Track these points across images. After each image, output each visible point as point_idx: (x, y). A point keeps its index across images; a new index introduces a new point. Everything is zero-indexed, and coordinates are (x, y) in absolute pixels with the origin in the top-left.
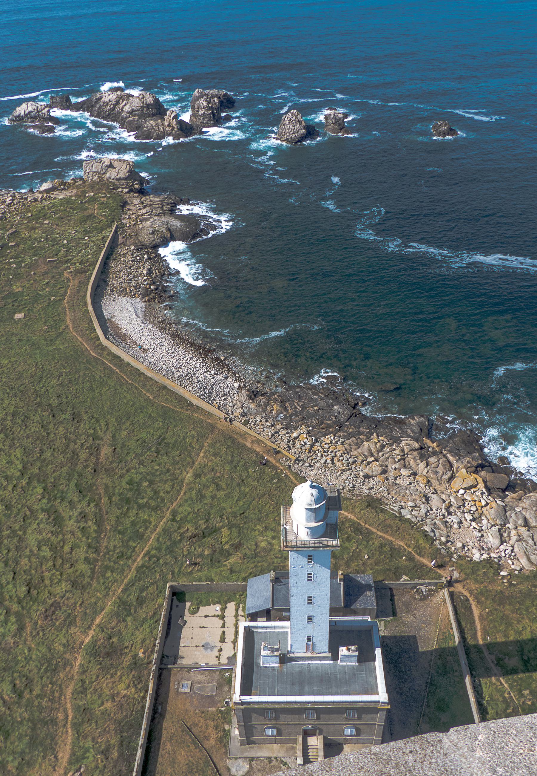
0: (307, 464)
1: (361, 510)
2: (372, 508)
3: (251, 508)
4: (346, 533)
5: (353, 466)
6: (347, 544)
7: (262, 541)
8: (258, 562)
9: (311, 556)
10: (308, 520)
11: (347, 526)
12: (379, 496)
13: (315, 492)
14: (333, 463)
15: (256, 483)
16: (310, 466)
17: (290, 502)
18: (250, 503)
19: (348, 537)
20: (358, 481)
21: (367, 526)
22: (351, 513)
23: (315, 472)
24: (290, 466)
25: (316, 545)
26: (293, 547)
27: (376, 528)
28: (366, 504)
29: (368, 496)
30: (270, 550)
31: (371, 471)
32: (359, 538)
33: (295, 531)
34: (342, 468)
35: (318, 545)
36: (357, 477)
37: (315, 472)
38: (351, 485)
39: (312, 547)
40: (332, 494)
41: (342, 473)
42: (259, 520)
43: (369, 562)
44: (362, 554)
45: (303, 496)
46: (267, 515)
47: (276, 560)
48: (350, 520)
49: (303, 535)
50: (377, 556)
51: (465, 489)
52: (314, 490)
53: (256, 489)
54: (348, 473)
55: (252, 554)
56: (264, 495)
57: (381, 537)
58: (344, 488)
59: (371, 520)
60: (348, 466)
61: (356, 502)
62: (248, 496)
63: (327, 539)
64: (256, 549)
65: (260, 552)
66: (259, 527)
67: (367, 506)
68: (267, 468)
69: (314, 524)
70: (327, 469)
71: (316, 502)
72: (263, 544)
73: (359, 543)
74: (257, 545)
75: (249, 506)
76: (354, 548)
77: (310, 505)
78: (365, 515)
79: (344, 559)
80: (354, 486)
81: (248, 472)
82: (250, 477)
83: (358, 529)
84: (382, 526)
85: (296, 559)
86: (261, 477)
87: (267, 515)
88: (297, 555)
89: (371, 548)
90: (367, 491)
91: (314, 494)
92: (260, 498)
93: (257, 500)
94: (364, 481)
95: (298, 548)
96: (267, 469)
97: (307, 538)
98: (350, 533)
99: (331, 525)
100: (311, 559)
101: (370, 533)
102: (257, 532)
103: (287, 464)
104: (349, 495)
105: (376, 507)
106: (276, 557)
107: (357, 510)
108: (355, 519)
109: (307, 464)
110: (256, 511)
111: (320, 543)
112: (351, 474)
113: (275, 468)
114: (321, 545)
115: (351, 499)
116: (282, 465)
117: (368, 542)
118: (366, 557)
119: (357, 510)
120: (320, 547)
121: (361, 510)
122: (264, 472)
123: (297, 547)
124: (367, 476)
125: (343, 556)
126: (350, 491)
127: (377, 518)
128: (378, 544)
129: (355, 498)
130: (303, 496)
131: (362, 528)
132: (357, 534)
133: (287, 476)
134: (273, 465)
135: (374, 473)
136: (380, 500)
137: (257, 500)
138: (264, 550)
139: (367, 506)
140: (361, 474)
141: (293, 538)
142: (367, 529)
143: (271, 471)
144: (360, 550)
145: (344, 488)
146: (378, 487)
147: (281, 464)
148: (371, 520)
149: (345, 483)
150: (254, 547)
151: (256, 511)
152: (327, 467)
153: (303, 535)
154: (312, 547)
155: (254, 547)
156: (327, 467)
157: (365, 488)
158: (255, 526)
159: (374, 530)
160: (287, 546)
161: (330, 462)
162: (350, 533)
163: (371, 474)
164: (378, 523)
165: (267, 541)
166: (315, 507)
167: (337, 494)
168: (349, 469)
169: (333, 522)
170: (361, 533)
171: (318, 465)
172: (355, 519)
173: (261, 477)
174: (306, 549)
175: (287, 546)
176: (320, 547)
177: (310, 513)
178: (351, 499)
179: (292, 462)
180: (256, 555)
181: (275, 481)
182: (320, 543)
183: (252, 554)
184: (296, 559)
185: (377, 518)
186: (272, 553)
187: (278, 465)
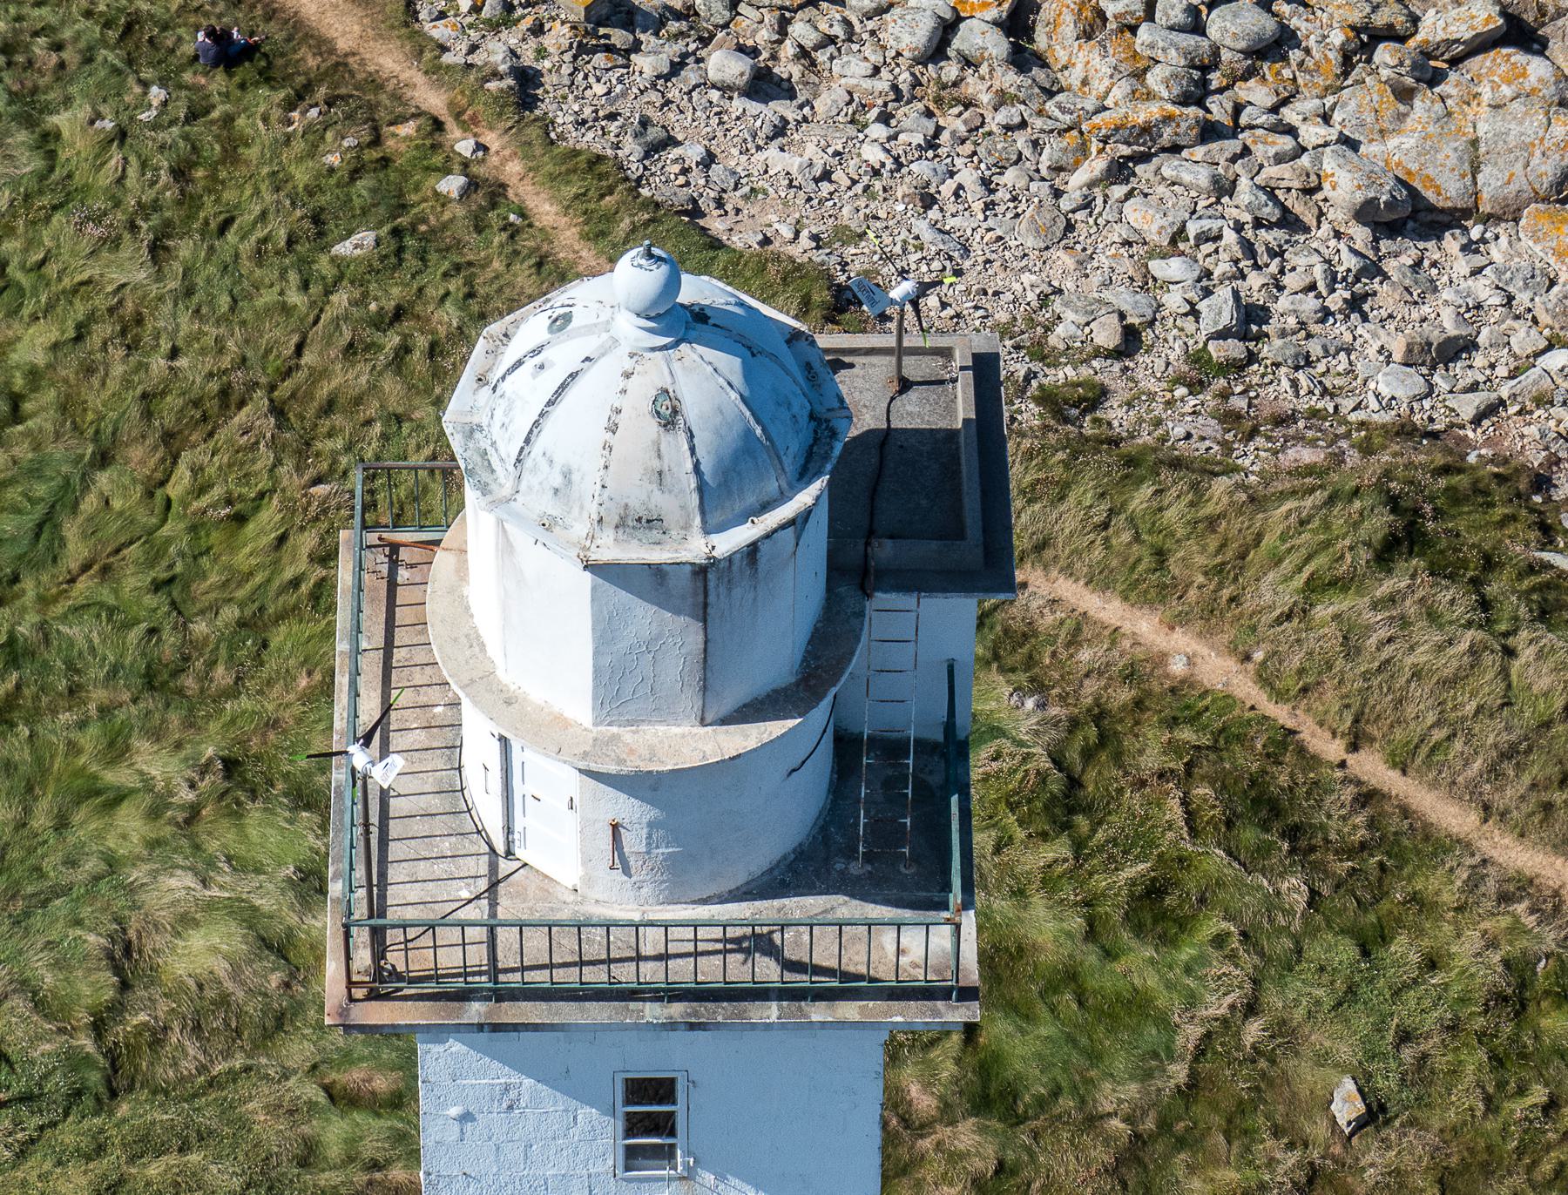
0: (723, 64)
1: (1316, 587)
2: (1442, 570)
3: (76, 550)
4: (1138, 841)
5: (1257, 94)
6: (1138, 966)
7: (186, 921)
8: (144, 1145)
9: (662, 1089)
10: (617, 688)
11: (1151, 760)
12: (1526, 439)
13: (707, 380)
14: (1023, 58)
15: (129, 269)
16: (763, 85)
17: (417, 494)
18: (66, 498)
19: (1152, 893)
20: (1305, 263)
21: (1371, 767)
22: (1209, 616)
23: (809, 151)
24: (526, 81)
25: (710, 971)
26: (451, 992)
27: (1472, 795)
28: (1380, 523)
29: (1406, 431)
30: (279, 1023)
31: (1450, 154)
32: (1273, 903)
33: (490, 814)
34: (1124, 108)
35: (738, 970)
36: (1289, 222)
37: (809, 151)
38: (1219, 310)
39: (672, 994)
40: (914, 413)
41: (1119, 171)
42: (155, 680)
43: (1374, 1159)
44: (1306, 1075)
45: (576, 408)
46: (254, 625)
47: (334, 1132)
48: (1183, 703)
49: (566, 854)
50: (1463, 1100)
51: (1105, 109)
52: (691, 353)
53: (131, 331)
54: (1193, 170)
55: (74, 1061)
56: (228, 400)
57: (1518, 888)
58: (1131, 341)
59: (1421, 709)
60: (1196, 95)
61: (1256, 501)
62: (41, 410)
63: (845, 907)
64: (117, 1009)
65: (156, 1037)
66: (154, 763)
67: (1386, 554)
68: (267, 99)
69: (687, 742)
70: (953, 122)
71: (718, 496)
72: (201, 954)
73: (1268, 955)
74: (126, 961)
75: (47, 525)
76: (1217, 1006)
77: (650, 523)
78: (1351, 650)
79: (1092, 1121)
80: (1251, 319)
81: (48, 142)
82: (69, 195)
83: (1266, 803)
84: (1539, 768)
85: (492, 1120)
86: (189, 202)
87: (254, 625)
88: (501, 1074)
89: (1404, 1012)
90: (1393, 385)
91: (694, 408)
92: (172, 442)
93: (140, 457)
94: (1373, 269)
95: (498, 998)
96: (260, 113)
97: (619, 900)
98: (1173, 836)
99: (892, 748)
100: (664, 1125)
101: (1397, 843)
102: (130, 824)
103: (495, 52)
104: (1190, 424)
105: (1490, 563)
106: (342, 1099)
107: (1273, 591)
108: (1246, 689)
109: (723, 64)
110: (133, 581)
111: (761, 943)
112: (1223, 188)
113: (354, 97)
114: (768, 970)
115: (1210, 470)
116: (435, 71)
117: (1369, 943)
118: (1346, 1106)
119: (1273, 591)
120: (760, 994)
121: (1316, 587)
122: (232, 148)
123: (501, 995)
124: (1408, 216)
125: (1083, 1091)
126: (1199, 372)
127: (1487, 684)
128: (1490, 973)
129: (1252, 458)
130: (576, 408)
131: (1318, 788)
132: (1254, 860)
133: (487, 193)
134: (339, 67)
135: (1492, 183)
136: (1542, 482)
137: (140, 457)
138: (209, 1013)
139: (1386, 554)
140: (1344, 186)
141: (461, 889)
142: (1368, 797)
143: (315, 136)
144: (1282, 1029)
145: (1131, 341)
146: (1524, 339)
147: (427, 52)
148: (1421, 709)
149: (1146, 282)
150: (95, 987)
151: (133, 581)
152: (953, 97)
153: (566, 854)
154: (672, 994)
155: (95, 987)
156: (953, 97)
157: (1370, 337)
158: (117, 750)
159: (1451, 816)
160: (382, 984)
161: (997, 45)
162: (1173, 836)
163: (1447, 189)
164: (1493, 734)
165: (248, 915)
166: (696, 547)
167: (962, 407)
168: (1209, 132)
169: (917, 716)
170: (1302, 842)
171: (850, 70)
172: (1246, 689)
173: (189, 202)
174: (598, 1013)
175: (382, 984)
176: (760, 994)
177: (644, 617)
178: (1210, 470)
179: (558, 36)
180: (118, 1076)
181: (357, 244)
182: (761, 943)
183: (74, 1061)
184: (492, 1120)
185: (1487, 684)
186: (298, 1050)
187: (389, 60)
